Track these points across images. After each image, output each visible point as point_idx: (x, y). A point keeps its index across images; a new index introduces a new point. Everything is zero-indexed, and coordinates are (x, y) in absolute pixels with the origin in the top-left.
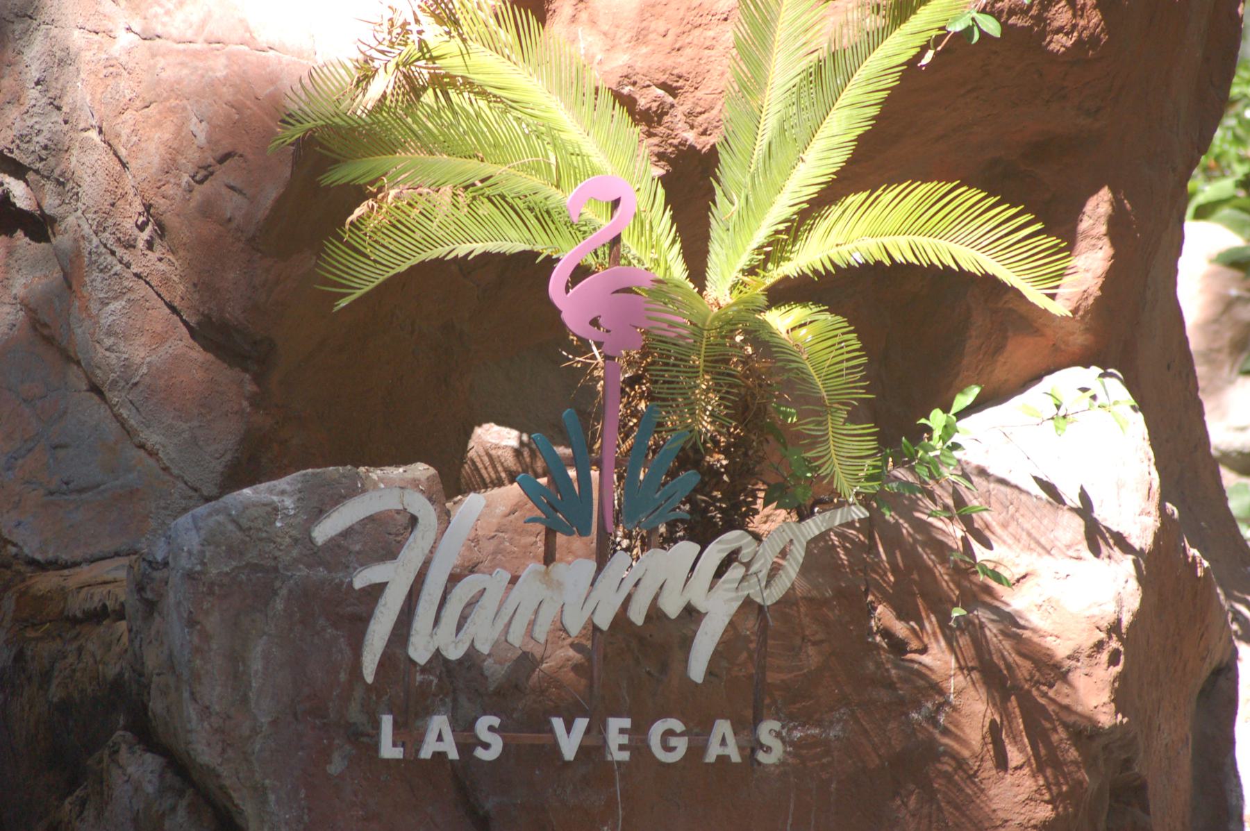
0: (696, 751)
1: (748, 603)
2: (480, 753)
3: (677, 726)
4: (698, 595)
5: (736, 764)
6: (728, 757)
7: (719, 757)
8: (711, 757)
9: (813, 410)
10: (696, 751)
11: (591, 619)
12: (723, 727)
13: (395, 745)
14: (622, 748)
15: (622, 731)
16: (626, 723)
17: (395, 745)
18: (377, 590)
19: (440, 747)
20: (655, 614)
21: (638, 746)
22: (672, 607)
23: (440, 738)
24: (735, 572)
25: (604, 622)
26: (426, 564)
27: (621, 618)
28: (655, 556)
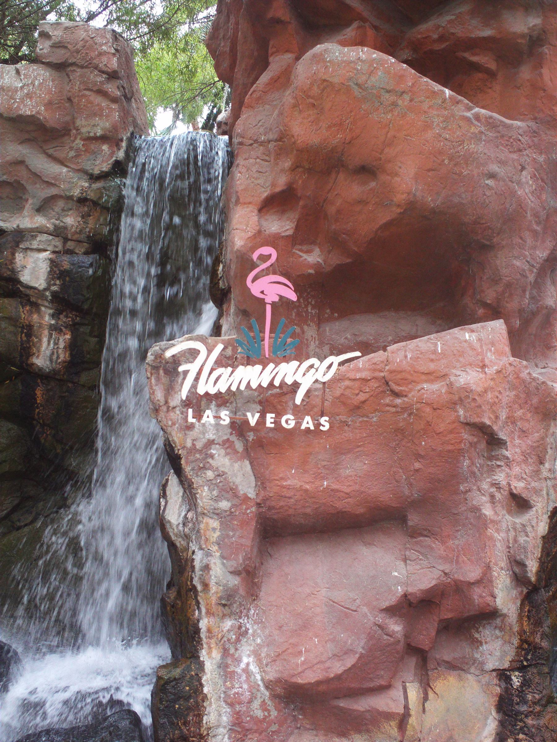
0: (298, 424)
1: (316, 381)
2: (321, 428)
3: (292, 417)
4: (298, 378)
5: (312, 430)
6: (309, 428)
7: (306, 428)
8: (303, 427)
9: (271, 331)
10: (298, 424)
11: (260, 384)
12: (308, 418)
13: (193, 418)
14: (271, 423)
15: (271, 418)
16: (273, 415)
17: (193, 418)
18: (186, 373)
19: (307, 426)
20: (283, 383)
21: (277, 422)
22: (289, 381)
23: (308, 423)
24: (313, 371)
25: (265, 384)
26: (202, 366)
27: (271, 384)
28: (283, 365)
